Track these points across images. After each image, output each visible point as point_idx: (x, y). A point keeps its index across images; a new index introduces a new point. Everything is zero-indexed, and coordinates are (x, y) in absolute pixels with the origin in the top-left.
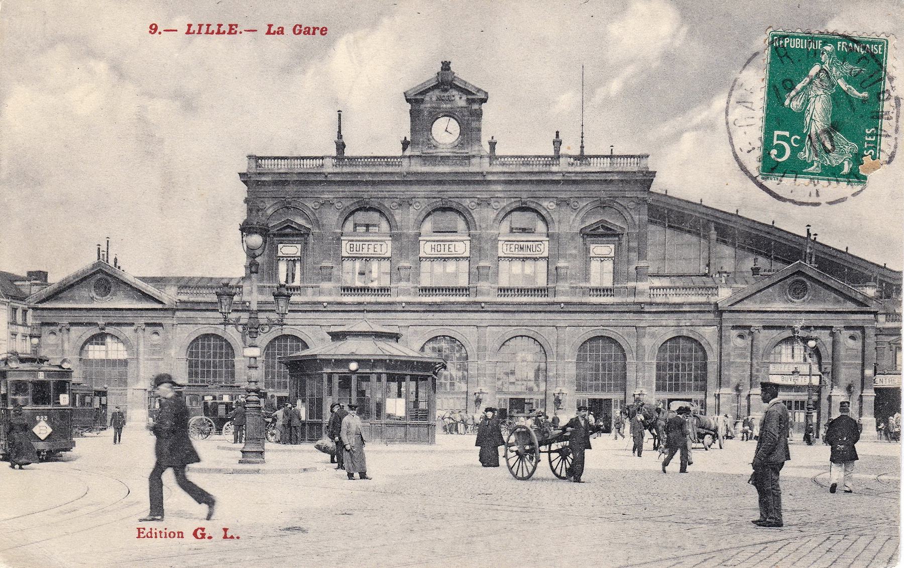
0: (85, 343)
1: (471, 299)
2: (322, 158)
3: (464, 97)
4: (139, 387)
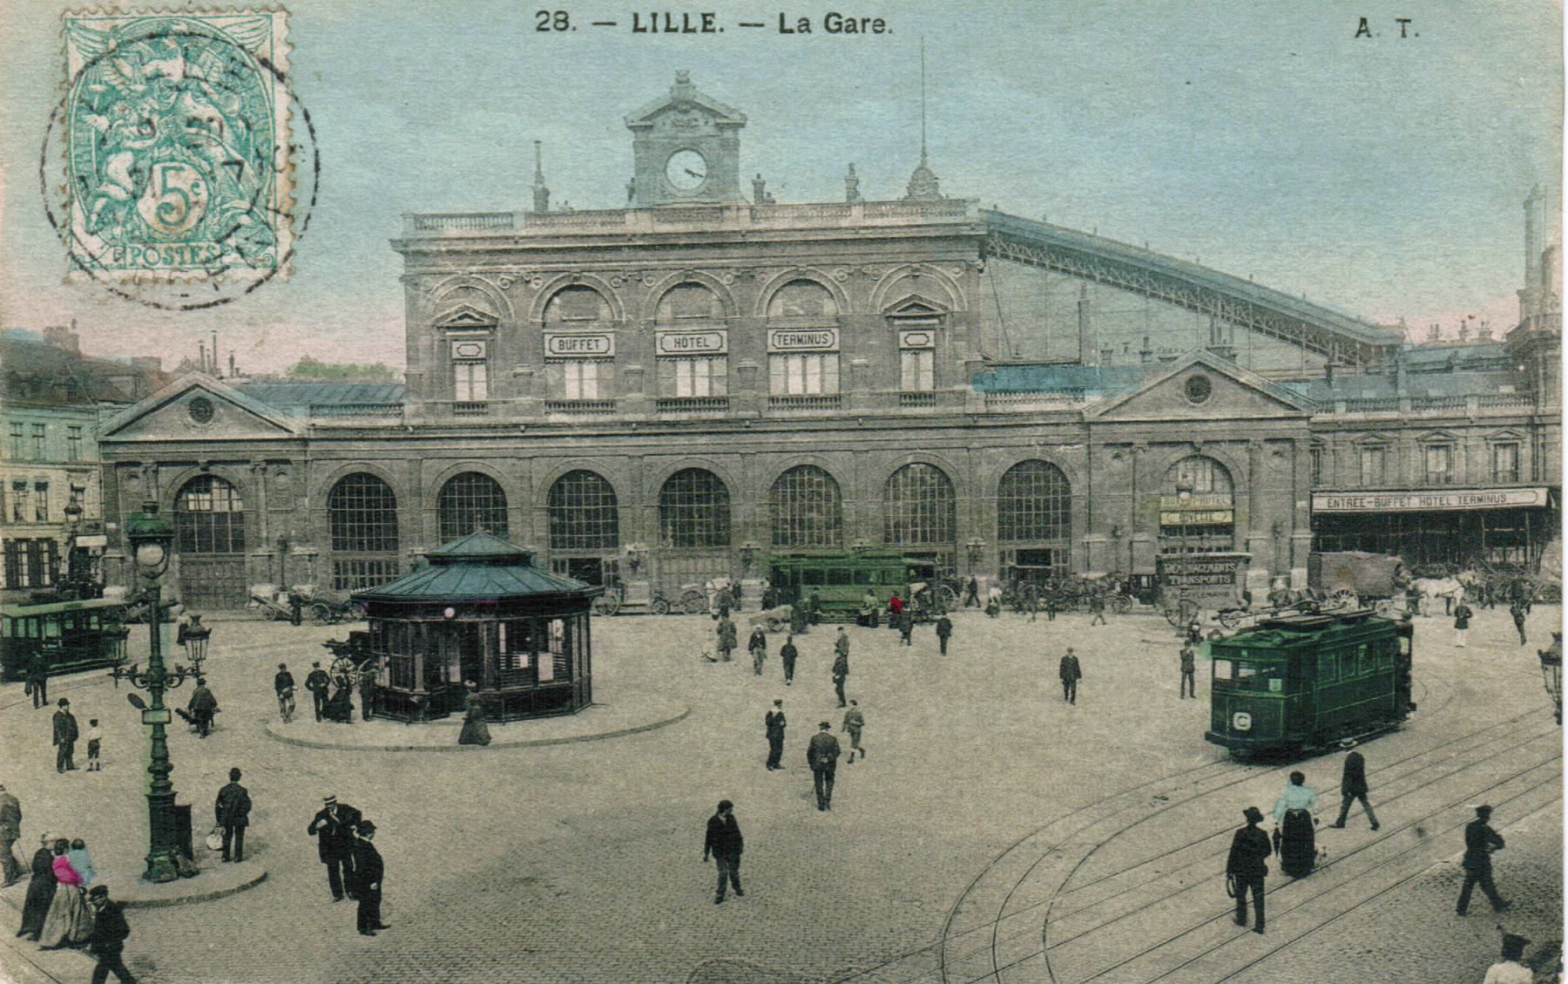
0: (181, 491)
2: (511, 215)
3: (712, 122)
4: (261, 553)
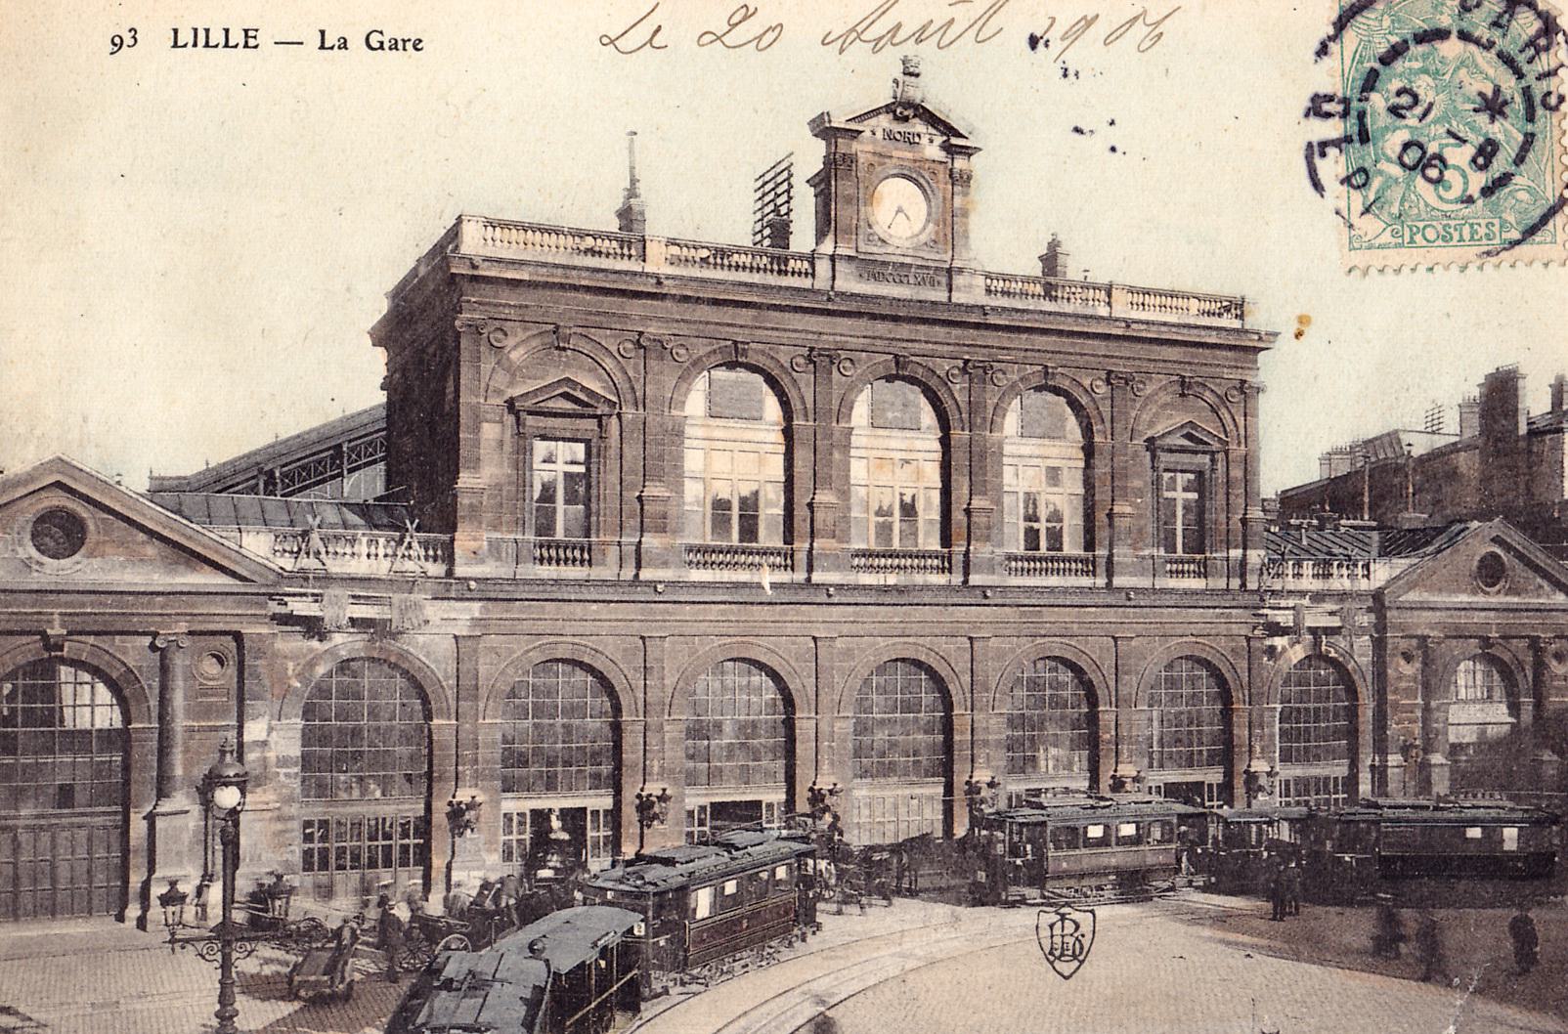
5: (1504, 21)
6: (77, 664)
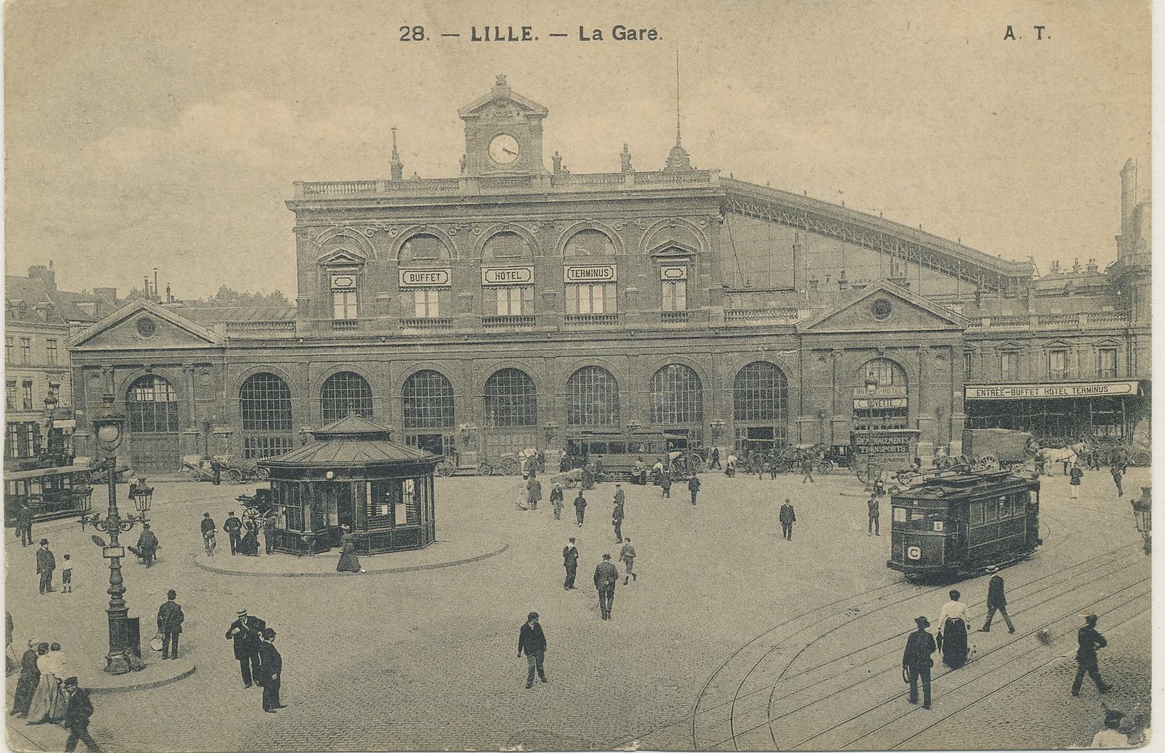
1: (620, 327)
3: (522, 113)
5: (1010, 33)
6: (161, 378)
